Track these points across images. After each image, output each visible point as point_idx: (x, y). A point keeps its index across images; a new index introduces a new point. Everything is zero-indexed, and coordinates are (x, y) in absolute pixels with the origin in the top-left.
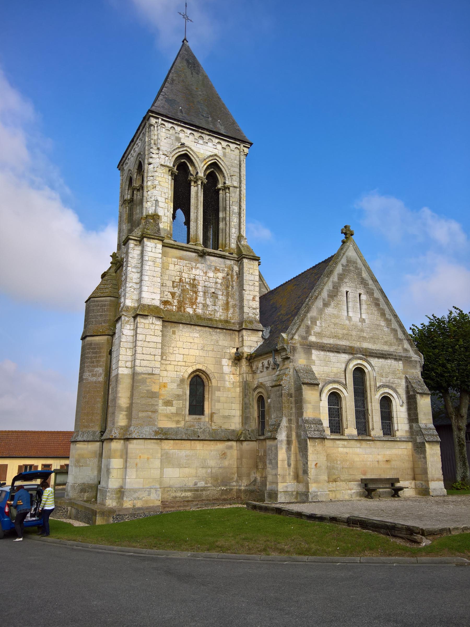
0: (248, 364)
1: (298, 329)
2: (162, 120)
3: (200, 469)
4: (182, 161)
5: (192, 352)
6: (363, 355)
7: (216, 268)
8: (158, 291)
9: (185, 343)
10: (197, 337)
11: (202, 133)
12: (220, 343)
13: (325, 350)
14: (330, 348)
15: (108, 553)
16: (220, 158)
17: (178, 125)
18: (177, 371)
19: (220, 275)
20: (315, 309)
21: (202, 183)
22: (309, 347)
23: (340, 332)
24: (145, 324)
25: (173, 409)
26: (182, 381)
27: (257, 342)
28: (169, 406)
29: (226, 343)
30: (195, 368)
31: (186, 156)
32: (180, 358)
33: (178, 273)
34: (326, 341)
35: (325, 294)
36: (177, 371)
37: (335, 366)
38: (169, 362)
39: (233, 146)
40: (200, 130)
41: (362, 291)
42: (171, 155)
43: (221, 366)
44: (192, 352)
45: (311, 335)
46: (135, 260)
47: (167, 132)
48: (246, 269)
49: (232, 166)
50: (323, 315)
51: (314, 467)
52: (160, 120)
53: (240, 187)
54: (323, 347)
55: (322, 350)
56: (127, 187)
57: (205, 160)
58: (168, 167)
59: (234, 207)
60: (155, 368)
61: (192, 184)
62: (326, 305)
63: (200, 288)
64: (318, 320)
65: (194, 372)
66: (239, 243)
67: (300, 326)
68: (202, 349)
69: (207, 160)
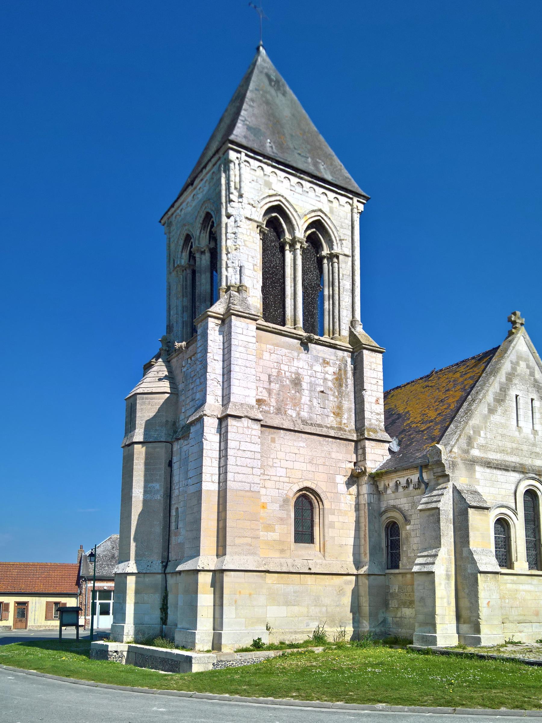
0: (371, 482)
1: (458, 440)
2: (247, 155)
3: (313, 608)
4: (274, 215)
5: (297, 465)
6: (536, 474)
7: (324, 361)
8: (254, 386)
9: (288, 454)
10: (304, 447)
11: (301, 178)
12: (334, 455)
13: (491, 467)
14: (497, 465)
15: (236, 705)
16: (326, 215)
17: (268, 165)
18: (278, 489)
19: (331, 370)
20: (478, 415)
21: (301, 247)
22: (472, 463)
23: (509, 445)
24: (237, 427)
25: (274, 536)
26: (286, 501)
27: (383, 456)
28: (270, 531)
29: (340, 456)
30: (301, 486)
31: (278, 209)
32: (282, 472)
33: (276, 364)
34: (492, 456)
35: (490, 398)
36: (278, 489)
37: (504, 487)
38: (268, 477)
39: (343, 200)
40: (298, 174)
41: (535, 396)
42: (260, 205)
43: (335, 484)
44: (297, 465)
45: (474, 448)
46: (217, 344)
47: (252, 172)
48: (367, 363)
49: (342, 227)
50: (488, 424)
51: (486, 605)
52: (243, 154)
53: (353, 256)
54: (489, 463)
55: (488, 467)
56: (181, 248)
57: (305, 215)
58: (256, 221)
59: (345, 282)
60: (253, 483)
61: (287, 247)
62: (492, 411)
63: (305, 386)
64: (482, 429)
65: (300, 490)
66: (353, 330)
67: (460, 436)
68: (310, 462)
69: (309, 216)
